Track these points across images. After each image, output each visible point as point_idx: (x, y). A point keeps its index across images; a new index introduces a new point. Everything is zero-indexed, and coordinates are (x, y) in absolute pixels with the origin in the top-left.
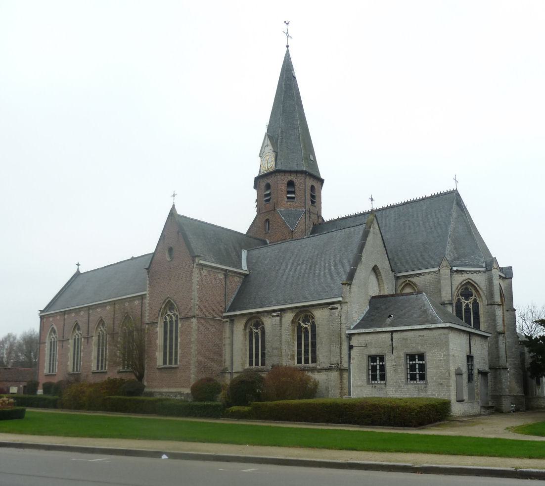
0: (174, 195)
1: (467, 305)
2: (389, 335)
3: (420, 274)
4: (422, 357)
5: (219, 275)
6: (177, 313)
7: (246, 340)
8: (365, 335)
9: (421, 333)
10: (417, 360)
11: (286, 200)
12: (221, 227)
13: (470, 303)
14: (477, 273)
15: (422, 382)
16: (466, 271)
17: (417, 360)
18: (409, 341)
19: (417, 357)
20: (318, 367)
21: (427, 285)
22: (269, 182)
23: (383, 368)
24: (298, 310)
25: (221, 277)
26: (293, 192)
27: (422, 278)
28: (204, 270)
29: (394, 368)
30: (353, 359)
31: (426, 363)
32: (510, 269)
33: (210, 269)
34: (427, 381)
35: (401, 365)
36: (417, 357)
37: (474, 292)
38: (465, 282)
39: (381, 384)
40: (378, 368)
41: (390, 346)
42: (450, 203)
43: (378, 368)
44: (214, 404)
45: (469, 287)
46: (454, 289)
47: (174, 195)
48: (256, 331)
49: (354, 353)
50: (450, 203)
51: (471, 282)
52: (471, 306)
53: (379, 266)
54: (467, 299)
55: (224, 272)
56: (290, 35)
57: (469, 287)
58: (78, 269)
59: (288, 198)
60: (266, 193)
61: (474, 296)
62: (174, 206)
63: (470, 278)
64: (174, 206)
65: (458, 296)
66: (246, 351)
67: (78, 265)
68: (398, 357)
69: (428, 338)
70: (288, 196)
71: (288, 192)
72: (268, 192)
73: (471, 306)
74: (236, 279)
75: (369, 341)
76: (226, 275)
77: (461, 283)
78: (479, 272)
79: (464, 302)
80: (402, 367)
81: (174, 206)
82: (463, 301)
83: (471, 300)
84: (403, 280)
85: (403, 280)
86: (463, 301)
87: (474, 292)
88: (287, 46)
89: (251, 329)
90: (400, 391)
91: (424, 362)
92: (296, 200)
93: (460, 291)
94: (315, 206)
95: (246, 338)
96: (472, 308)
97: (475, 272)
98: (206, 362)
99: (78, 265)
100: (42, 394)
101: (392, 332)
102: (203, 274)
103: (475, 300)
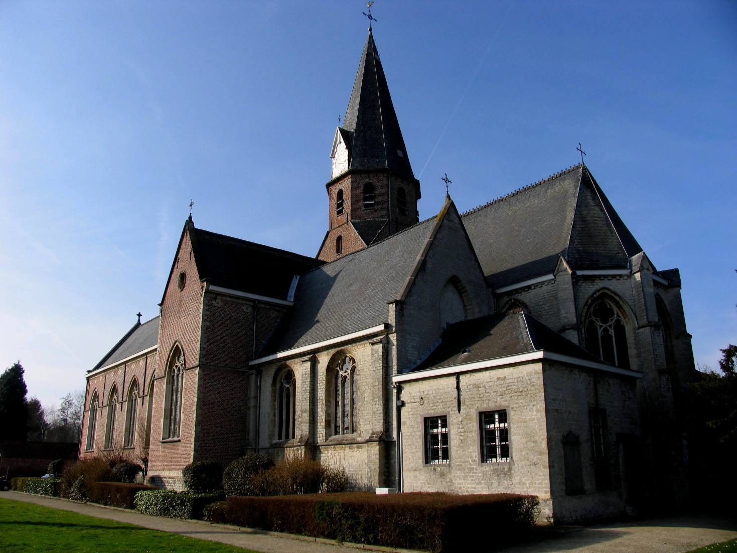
1: (606, 331)
2: (453, 380)
3: (529, 287)
4: (503, 416)
5: (244, 308)
7: (275, 401)
12: (287, 252)
13: (610, 326)
14: (618, 278)
15: (504, 459)
16: (599, 277)
18: (482, 390)
19: (496, 416)
20: (360, 439)
21: (541, 303)
22: (341, 188)
23: (504, 434)
24: (332, 351)
25: (248, 311)
27: (533, 292)
28: (217, 300)
29: (462, 438)
30: (405, 423)
31: (449, 431)
32: (675, 272)
33: (228, 299)
34: (512, 458)
35: (471, 432)
36: (496, 416)
37: (615, 309)
38: (598, 294)
39: (443, 465)
41: (455, 398)
42: (678, 269)
45: (608, 301)
46: (581, 306)
48: (287, 386)
49: (404, 411)
50: (678, 269)
51: (609, 293)
52: (612, 332)
54: (605, 321)
55: (251, 304)
57: (608, 301)
58: (139, 320)
59: (366, 206)
61: (615, 315)
62: (190, 218)
63: (606, 286)
64: (190, 218)
65: (590, 316)
66: (275, 416)
67: (139, 315)
68: (468, 417)
69: (511, 381)
71: (366, 199)
73: (612, 332)
74: (274, 314)
75: (426, 393)
76: (254, 307)
77: (592, 296)
78: (621, 276)
79: (600, 326)
80: (473, 434)
84: (506, 299)
85: (506, 299)
86: (599, 324)
87: (615, 309)
88: (371, 30)
90: (470, 477)
91: (506, 425)
92: (376, 207)
93: (592, 309)
94: (406, 215)
95: (275, 397)
96: (613, 334)
97: (614, 276)
98: (217, 433)
101: (458, 375)
102: (216, 305)
103: (618, 321)
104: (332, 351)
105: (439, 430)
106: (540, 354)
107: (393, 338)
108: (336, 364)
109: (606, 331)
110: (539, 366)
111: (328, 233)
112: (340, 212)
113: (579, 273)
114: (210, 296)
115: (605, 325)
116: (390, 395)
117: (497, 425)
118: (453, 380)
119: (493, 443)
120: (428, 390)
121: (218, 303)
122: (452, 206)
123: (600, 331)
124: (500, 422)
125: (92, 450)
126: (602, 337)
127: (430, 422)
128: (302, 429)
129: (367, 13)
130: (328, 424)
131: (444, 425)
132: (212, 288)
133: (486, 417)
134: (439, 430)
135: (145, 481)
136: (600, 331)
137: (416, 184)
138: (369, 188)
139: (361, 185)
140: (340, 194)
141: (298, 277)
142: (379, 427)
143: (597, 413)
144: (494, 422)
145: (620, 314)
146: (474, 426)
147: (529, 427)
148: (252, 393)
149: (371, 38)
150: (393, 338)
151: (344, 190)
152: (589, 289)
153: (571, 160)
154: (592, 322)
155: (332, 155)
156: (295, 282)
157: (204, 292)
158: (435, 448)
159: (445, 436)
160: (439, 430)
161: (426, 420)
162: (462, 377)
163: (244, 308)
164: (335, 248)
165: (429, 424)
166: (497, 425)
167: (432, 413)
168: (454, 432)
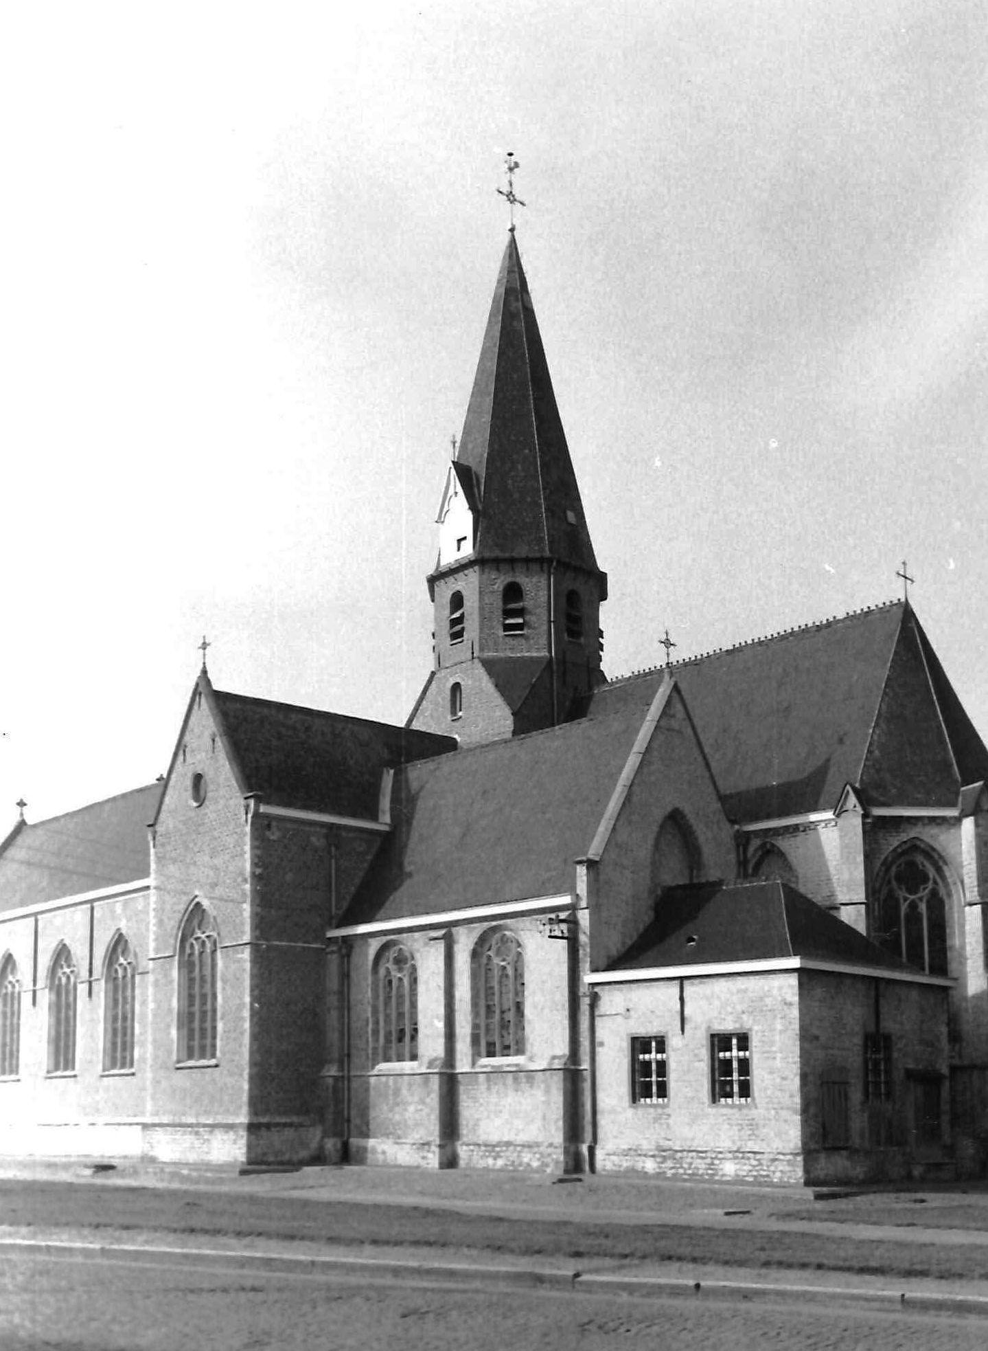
0: (205, 646)
6: (214, 934)
8: (722, 981)
9: (741, 982)
10: (734, 1047)
11: (501, 633)
13: (921, 899)
15: (743, 1100)
17: (734, 1047)
22: (458, 588)
23: (745, 1066)
26: (520, 612)
33: (289, 825)
34: (754, 1099)
37: (932, 872)
40: (735, 1065)
43: (735, 1065)
44: (817, 1189)
47: (205, 646)
52: (923, 907)
53: (687, 809)
56: (518, 197)
57: (919, 859)
59: (507, 627)
60: (454, 616)
61: (931, 882)
64: (204, 672)
70: (507, 622)
71: (508, 613)
72: (457, 615)
73: (923, 907)
81: (204, 672)
82: (902, 894)
83: (924, 893)
88: (512, 230)
89: (388, 971)
91: (747, 1053)
97: (933, 820)
99: (22, 804)
100: (790, 1172)
101: (682, 979)
103: (934, 894)
104: (480, 928)
105: (653, 1056)
106: (795, 962)
107: (584, 917)
108: (487, 947)
109: (913, 906)
110: (793, 980)
111: (433, 674)
112: (457, 635)
113: (878, 812)
114: (261, 825)
115: (912, 897)
116: (580, 1006)
117: (735, 1052)
118: (674, 989)
119: (729, 1074)
120: (639, 1002)
121: (274, 835)
122: (675, 694)
123: (904, 908)
124: (739, 1049)
125: (133, 1070)
126: (907, 915)
127: (640, 1044)
128: (431, 1043)
129: (505, 189)
130: (475, 1040)
131: (661, 1049)
132: (263, 809)
133: (720, 1041)
134: (653, 1055)
135: (238, 1121)
136: (904, 908)
137: (603, 577)
138: (513, 592)
139: (499, 586)
140: (457, 601)
141: (392, 772)
142: (563, 1049)
143: (877, 1042)
144: (730, 1050)
145: (939, 880)
146: (705, 1053)
147: (777, 1068)
148: (333, 983)
149: (513, 244)
150: (584, 917)
151: (464, 593)
152: (894, 842)
153: (894, 593)
154: (891, 891)
155: (440, 517)
156: (388, 778)
157: (250, 816)
158: (648, 1080)
159: (662, 1066)
160: (653, 1056)
161: (634, 1040)
162: (689, 989)
163: (313, 839)
164: (448, 705)
165: (638, 1046)
166: (735, 1052)
167: (642, 1031)
168: (674, 1060)
